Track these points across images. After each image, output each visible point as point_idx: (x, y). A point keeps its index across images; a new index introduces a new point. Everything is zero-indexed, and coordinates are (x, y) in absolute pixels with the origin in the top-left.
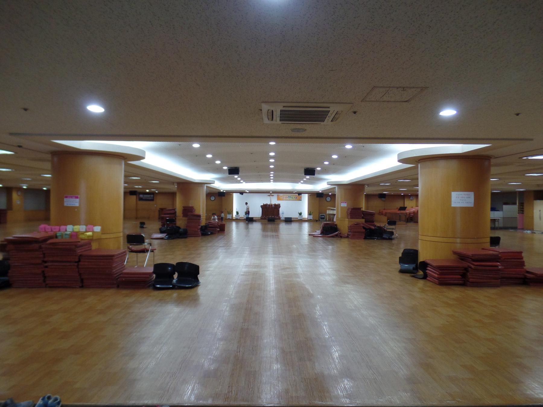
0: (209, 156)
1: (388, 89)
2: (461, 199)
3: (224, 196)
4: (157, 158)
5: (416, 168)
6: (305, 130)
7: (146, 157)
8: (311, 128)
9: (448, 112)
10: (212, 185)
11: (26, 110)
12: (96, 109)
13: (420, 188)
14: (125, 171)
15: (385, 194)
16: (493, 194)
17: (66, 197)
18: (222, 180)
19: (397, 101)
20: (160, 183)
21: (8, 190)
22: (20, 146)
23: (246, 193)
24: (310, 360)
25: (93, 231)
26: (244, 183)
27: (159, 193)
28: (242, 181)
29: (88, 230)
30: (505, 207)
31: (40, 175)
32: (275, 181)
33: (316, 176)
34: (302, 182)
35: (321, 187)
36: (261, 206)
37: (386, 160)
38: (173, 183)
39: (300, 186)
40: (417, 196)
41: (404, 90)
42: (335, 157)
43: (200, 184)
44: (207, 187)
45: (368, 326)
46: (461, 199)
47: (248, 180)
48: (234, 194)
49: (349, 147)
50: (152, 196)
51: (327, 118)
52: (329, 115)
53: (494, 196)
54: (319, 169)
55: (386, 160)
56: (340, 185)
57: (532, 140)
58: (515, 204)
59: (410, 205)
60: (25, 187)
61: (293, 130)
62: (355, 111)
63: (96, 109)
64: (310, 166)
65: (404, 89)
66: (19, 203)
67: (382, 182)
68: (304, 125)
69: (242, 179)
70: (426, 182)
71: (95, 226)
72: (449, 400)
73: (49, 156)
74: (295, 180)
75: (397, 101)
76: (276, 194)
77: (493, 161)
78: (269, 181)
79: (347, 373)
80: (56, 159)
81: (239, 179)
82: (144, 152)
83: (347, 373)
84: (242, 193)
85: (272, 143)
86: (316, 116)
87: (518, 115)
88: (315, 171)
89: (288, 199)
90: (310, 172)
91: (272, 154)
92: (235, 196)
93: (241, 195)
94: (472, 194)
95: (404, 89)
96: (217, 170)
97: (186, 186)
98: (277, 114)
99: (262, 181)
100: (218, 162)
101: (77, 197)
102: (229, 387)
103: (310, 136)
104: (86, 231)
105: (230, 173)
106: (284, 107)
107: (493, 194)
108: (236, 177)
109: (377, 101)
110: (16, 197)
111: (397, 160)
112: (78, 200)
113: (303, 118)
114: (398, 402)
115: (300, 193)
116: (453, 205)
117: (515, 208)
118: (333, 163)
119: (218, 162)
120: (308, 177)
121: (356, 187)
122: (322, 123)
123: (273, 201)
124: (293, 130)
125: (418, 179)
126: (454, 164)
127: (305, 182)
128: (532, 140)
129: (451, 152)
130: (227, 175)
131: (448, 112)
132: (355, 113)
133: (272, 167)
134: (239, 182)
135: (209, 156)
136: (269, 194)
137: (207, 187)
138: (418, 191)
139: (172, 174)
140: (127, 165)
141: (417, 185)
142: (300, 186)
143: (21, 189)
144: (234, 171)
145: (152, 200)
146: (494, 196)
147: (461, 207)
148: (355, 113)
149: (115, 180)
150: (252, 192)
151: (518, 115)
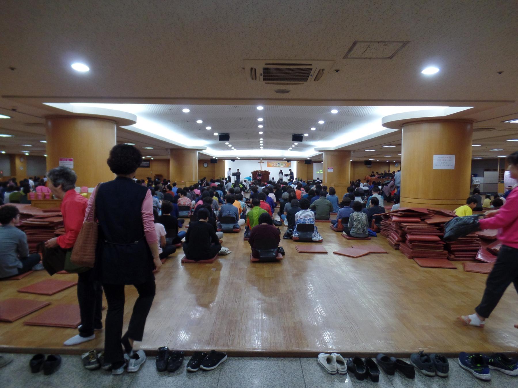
0: (200, 122)
1: (369, 44)
2: (442, 162)
3: (216, 163)
4: (147, 121)
5: (400, 132)
6: (287, 92)
7: (137, 122)
8: (296, 89)
9: (430, 71)
10: (204, 152)
11: (13, 69)
12: (80, 67)
13: (403, 155)
14: (118, 136)
15: (370, 161)
16: (474, 162)
17: (61, 160)
18: (214, 146)
19: (379, 58)
20: (154, 149)
21: (11, 157)
22: (14, 110)
23: (237, 159)
24: (290, 311)
25: (87, 192)
26: (235, 150)
27: (154, 160)
28: (233, 148)
29: (82, 191)
30: (486, 173)
31: (39, 141)
32: (265, 147)
33: (304, 142)
34: (291, 148)
35: (308, 153)
36: (252, 173)
37: (372, 123)
38: (167, 149)
39: (289, 153)
40: (400, 162)
41: (385, 45)
42: (321, 122)
43: (193, 150)
44: (199, 153)
45: (347, 280)
46: (442, 162)
47: (238, 146)
48: (226, 161)
49: (334, 111)
50: (148, 163)
51: (310, 77)
52: (312, 73)
53: (475, 162)
54: (306, 135)
55: (372, 123)
56: (327, 152)
57: (514, 102)
58: (496, 170)
59: (392, 169)
60: (27, 154)
61: (278, 91)
62: (337, 69)
63: (80, 67)
64: (298, 132)
65: (385, 43)
66: (22, 169)
67: (368, 148)
68: (288, 86)
69: (233, 146)
70: (411, 146)
71: (89, 187)
72: (422, 347)
73: (43, 121)
74: (284, 147)
75: (379, 58)
76: (267, 161)
77: (475, 125)
78: (258, 147)
79: (327, 325)
80: (50, 123)
81: (230, 146)
82: (135, 117)
83: (327, 325)
84: (233, 159)
85: (260, 108)
86: (297, 74)
87: (500, 73)
88: (302, 137)
89: (277, 165)
90: (298, 138)
91: (260, 120)
92: (226, 161)
93: (232, 162)
94: (453, 157)
95: (385, 43)
96: (208, 136)
97: (178, 153)
98: (259, 71)
99: (252, 148)
100: (209, 128)
101: (71, 160)
102: (211, 334)
103: (295, 97)
104: (81, 193)
105: (220, 140)
106: (266, 64)
107: (474, 162)
108: (227, 143)
109: (360, 58)
110: (18, 162)
111: (381, 123)
112: (72, 163)
113: (286, 77)
114: (372, 348)
115: (289, 160)
116: (434, 168)
117: (496, 174)
118: (320, 129)
119: (209, 128)
120: (296, 144)
121: (342, 154)
122: (305, 82)
123: (263, 167)
124: (278, 91)
125: (401, 145)
126: (437, 127)
127: (294, 149)
128: (514, 102)
129: (434, 116)
130: (218, 142)
131: (430, 71)
132: (337, 71)
133: (261, 133)
134: (230, 149)
135: (200, 122)
136: (259, 161)
137: (199, 153)
138: (400, 158)
139: (164, 140)
140: (119, 130)
141: (400, 152)
142: (289, 153)
143: (23, 156)
144: (224, 137)
145: (148, 167)
146: (475, 162)
147: (442, 171)
148: (337, 71)
149: (107, 141)
150: (243, 159)
151: (500, 73)
